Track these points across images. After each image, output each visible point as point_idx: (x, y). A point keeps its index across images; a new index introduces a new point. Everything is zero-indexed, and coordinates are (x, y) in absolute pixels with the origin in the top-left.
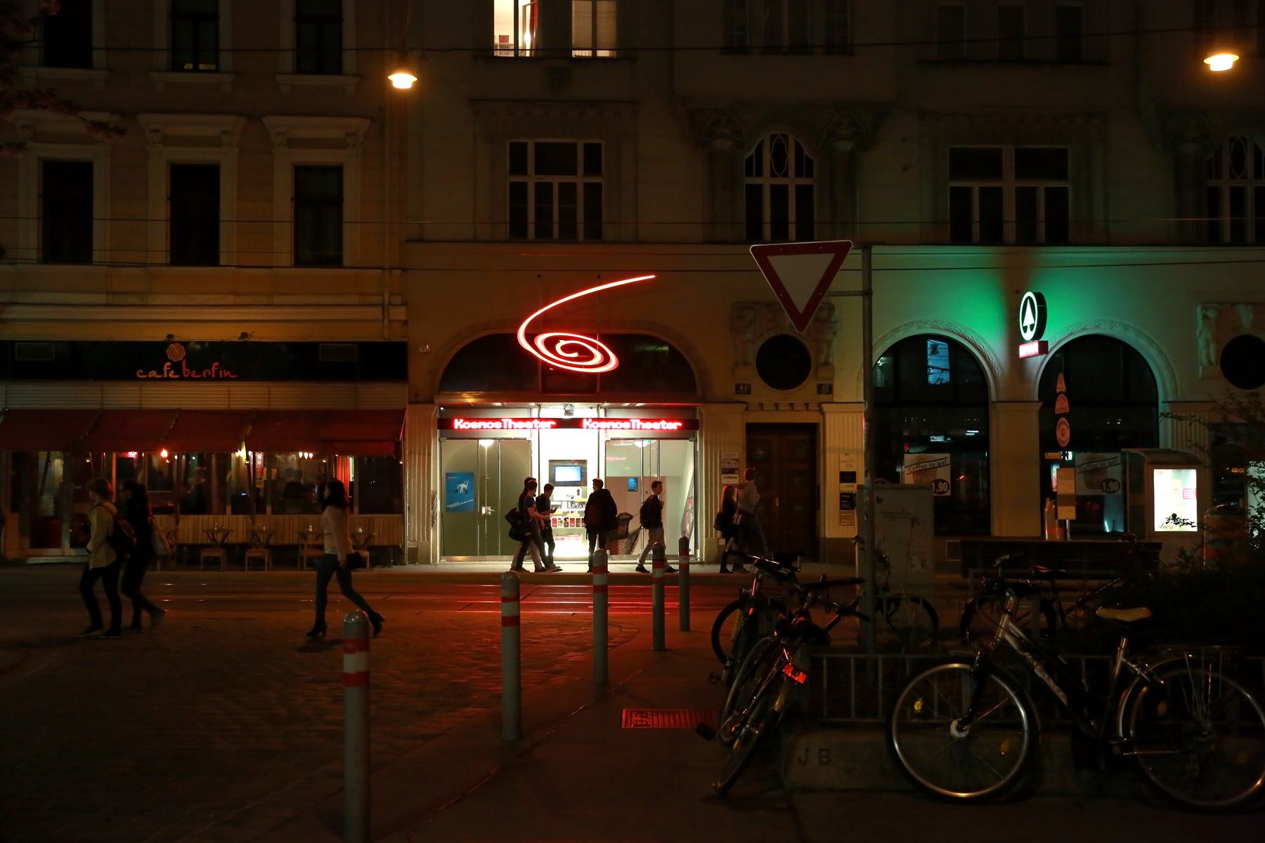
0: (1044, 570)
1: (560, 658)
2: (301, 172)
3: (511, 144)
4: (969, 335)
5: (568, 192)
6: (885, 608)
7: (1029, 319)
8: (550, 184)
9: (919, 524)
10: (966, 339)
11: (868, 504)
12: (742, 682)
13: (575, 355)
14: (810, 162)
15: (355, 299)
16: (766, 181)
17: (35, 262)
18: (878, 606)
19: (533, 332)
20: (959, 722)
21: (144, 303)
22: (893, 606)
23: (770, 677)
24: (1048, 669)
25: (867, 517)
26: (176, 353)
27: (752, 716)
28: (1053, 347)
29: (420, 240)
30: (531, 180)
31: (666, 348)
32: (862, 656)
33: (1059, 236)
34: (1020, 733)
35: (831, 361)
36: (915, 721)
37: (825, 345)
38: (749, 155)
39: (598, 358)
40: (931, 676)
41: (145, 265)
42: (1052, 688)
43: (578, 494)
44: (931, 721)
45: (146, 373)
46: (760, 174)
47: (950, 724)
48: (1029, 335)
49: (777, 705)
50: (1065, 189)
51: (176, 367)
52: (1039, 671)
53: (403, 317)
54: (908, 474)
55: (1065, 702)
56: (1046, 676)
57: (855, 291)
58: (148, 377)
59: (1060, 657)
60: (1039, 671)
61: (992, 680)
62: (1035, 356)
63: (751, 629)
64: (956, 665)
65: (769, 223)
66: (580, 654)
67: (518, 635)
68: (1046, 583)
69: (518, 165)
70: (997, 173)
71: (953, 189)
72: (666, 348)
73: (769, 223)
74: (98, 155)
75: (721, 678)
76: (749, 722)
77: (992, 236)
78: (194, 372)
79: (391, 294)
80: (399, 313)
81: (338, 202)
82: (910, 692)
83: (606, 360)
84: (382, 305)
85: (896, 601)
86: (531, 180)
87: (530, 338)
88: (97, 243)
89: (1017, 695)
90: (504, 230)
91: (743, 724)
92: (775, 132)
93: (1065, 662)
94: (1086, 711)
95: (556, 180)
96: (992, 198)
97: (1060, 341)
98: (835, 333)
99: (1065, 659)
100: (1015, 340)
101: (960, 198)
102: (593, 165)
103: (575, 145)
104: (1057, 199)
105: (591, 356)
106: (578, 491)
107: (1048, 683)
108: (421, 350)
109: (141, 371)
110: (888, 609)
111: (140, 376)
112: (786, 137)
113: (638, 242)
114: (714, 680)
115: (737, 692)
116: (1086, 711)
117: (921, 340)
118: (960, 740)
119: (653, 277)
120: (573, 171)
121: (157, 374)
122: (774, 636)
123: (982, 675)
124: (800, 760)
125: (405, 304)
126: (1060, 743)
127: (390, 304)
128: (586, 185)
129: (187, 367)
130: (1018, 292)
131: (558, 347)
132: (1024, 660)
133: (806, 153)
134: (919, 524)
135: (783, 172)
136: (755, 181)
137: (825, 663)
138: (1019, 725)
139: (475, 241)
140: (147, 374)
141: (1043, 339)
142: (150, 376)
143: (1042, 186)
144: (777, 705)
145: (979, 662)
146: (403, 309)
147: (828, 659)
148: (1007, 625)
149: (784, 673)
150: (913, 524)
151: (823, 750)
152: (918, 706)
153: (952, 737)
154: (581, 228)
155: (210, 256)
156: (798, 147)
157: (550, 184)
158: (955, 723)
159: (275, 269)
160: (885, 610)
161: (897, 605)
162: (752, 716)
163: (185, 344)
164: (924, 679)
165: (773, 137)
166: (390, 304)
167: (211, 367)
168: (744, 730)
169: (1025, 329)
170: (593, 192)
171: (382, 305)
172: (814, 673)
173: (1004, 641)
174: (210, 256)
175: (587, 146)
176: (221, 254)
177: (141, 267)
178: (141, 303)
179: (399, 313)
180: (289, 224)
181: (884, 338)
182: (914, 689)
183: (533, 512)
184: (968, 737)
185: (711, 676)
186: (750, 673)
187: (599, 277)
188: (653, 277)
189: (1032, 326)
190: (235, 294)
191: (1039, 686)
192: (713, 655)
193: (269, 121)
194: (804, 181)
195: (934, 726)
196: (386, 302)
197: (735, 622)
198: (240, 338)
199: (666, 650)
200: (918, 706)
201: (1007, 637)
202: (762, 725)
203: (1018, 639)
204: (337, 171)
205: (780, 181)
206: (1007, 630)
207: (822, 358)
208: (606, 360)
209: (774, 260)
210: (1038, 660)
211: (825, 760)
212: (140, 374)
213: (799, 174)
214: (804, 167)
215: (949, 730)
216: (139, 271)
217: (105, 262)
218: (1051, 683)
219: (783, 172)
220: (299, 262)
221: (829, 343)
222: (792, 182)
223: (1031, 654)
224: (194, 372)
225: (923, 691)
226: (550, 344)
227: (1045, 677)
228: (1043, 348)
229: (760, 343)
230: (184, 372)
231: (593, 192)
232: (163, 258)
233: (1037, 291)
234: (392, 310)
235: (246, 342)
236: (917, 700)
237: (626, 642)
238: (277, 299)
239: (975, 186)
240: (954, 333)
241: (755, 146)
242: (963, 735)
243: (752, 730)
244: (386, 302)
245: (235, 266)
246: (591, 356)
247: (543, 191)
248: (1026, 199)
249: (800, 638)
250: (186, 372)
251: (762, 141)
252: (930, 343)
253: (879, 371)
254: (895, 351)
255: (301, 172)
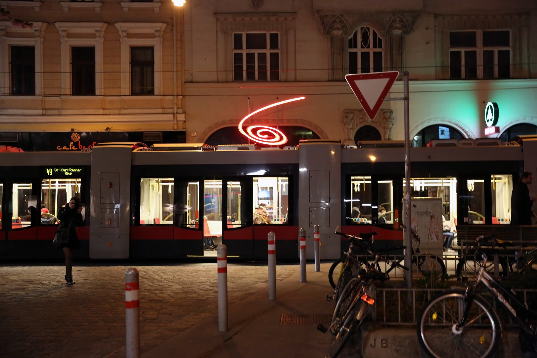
0: (500, 242)
1: (254, 286)
2: (133, 49)
3: (235, 35)
4: (460, 124)
5: (262, 57)
6: (417, 261)
7: (490, 116)
8: (254, 54)
9: (434, 218)
10: (458, 126)
11: (408, 208)
12: (342, 301)
13: (266, 136)
14: (380, 40)
15: (160, 111)
16: (359, 50)
17: (8, 94)
18: (414, 261)
19: (246, 125)
20: (457, 326)
21: (60, 114)
22: (421, 260)
23: (355, 301)
24: (506, 297)
25: (407, 215)
26: (75, 138)
27: (346, 321)
28: (502, 130)
29: (191, 82)
30: (244, 52)
31: (311, 133)
32: (405, 290)
33: (505, 75)
34: (490, 332)
35: (391, 138)
36: (433, 324)
37: (389, 130)
38: (350, 38)
39: (277, 137)
40: (442, 301)
41: (60, 95)
42: (508, 308)
43: (269, 204)
44: (442, 324)
45: (61, 147)
46: (356, 47)
47: (452, 326)
48: (490, 124)
49: (358, 316)
50: (508, 51)
51: (76, 144)
52: (500, 298)
53: (184, 119)
54: (430, 193)
55: (515, 315)
56: (505, 301)
57: (400, 98)
58: (62, 149)
59: (512, 290)
60: (500, 298)
61: (475, 303)
62: (493, 134)
63: (347, 274)
64: (455, 295)
65: (360, 69)
66: (264, 284)
67: (226, 277)
68: (501, 248)
69: (238, 44)
70: (474, 44)
71: (451, 52)
72: (311, 133)
73: (360, 69)
74: (37, 43)
75: (332, 298)
76: (344, 324)
77: (471, 75)
78: (84, 146)
79: (178, 108)
80: (181, 117)
81: (151, 63)
82: (430, 309)
83: (282, 138)
84: (174, 113)
85: (424, 258)
86: (244, 52)
87: (245, 128)
88: (37, 85)
89: (489, 311)
90: (231, 76)
91: (341, 326)
92: (362, 26)
93: (515, 293)
94: (527, 320)
95: (256, 52)
96: (471, 56)
97: (506, 126)
98: (393, 125)
99: (515, 292)
100: (483, 125)
101: (455, 56)
102: (274, 44)
103: (265, 34)
104: (504, 55)
105: (274, 137)
106: (269, 202)
107: (506, 305)
108: (192, 135)
109: (59, 147)
110: (419, 261)
111: (58, 149)
112: (368, 29)
113: (296, 81)
114: (329, 299)
115: (339, 306)
116: (527, 320)
117: (436, 127)
118: (458, 335)
119: (303, 98)
120: (265, 47)
121: (67, 148)
122: (358, 278)
123: (469, 301)
124: (371, 345)
125: (184, 113)
126: (512, 337)
127: (177, 113)
128: (271, 54)
129: (81, 145)
130: (484, 102)
131: (258, 132)
132: (492, 292)
133: (378, 35)
134: (434, 218)
135: (367, 45)
136: (353, 50)
137: (384, 293)
138: (491, 327)
139: (218, 82)
140: (62, 148)
141: (497, 125)
142: (63, 149)
143: (496, 50)
144: (358, 316)
145: (467, 293)
146: (183, 116)
147: (387, 292)
148: (483, 273)
149: (362, 300)
150: (431, 219)
151: (384, 340)
152: (435, 316)
153: (453, 334)
154: (268, 73)
155: (90, 91)
156: (375, 34)
157: (254, 54)
158: (454, 327)
159: (122, 97)
160: (417, 263)
161: (424, 260)
162: (346, 321)
163: (80, 133)
164: (438, 302)
165: (362, 29)
166: (177, 113)
167: (92, 144)
168: (341, 329)
169: (488, 121)
170: (274, 57)
171: (174, 113)
172: (378, 299)
173: (481, 282)
174: (90, 91)
175: (271, 35)
176: (96, 89)
177: (58, 96)
178: (58, 114)
179: (181, 117)
180: (129, 73)
181: (417, 127)
182: (433, 306)
183: (426, 191)
184: (462, 334)
185: (327, 297)
186: (347, 296)
187: (277, 98)
188: (303, 98)
189: (491, 120)
190: (103, 109)
191: (500, 305)
192: (329, 284)
193: (117, 25)
194: (378, 50)
195: (443, 327)
196: (175, 112)
197: (339, 268)
198: (106, 130)
199: (307, 282)
200: (435, 316)
201: (483, 280)
202: (351, 326)
203: (489, 281)
204: (151, 49)
205: (365, 50)
206: (483, 276)
207: (387, 137)
208: (282, 138)
209: (358, 83)
210: (501, 292)
211: (384, 345)
212: (59, 148)
213: (375, 46)
214: (377, 43)
215: (451, 330)
216: (57, 98)
217: (41, 94)
218: (507, 305)
219: (367, 45)
220: (133, 93)
221: (390, 129)
222: (371, 51)
223: (496, 289)
224: (84, 146)
225: (438, 309)
226: (254, 131)
227: (504, 301)
228: (497, 130)
229: (356, 130)
230: (79, 147)
231: (274, 57)
232: (68, 91)
233: (494, 102)
234: (178, 116)
235: (109, 132)
236: (434, 313)
237: (288, 277)
238: (123, 111)
239: (463, 51)
240: (452, 123)
241: (353, 34)
242: (459, 332)
243: (346, 329)
244: (175, 112)
245: (103, 95)
246: (274, 137)
247: (250, 57)
248: (488, 56)
249: (371, 280)
250: (81, 147)
251: (357, 31)
252: (441, 128)
253: (415, 143)
254: (423, 133)
255: (133, 49)
